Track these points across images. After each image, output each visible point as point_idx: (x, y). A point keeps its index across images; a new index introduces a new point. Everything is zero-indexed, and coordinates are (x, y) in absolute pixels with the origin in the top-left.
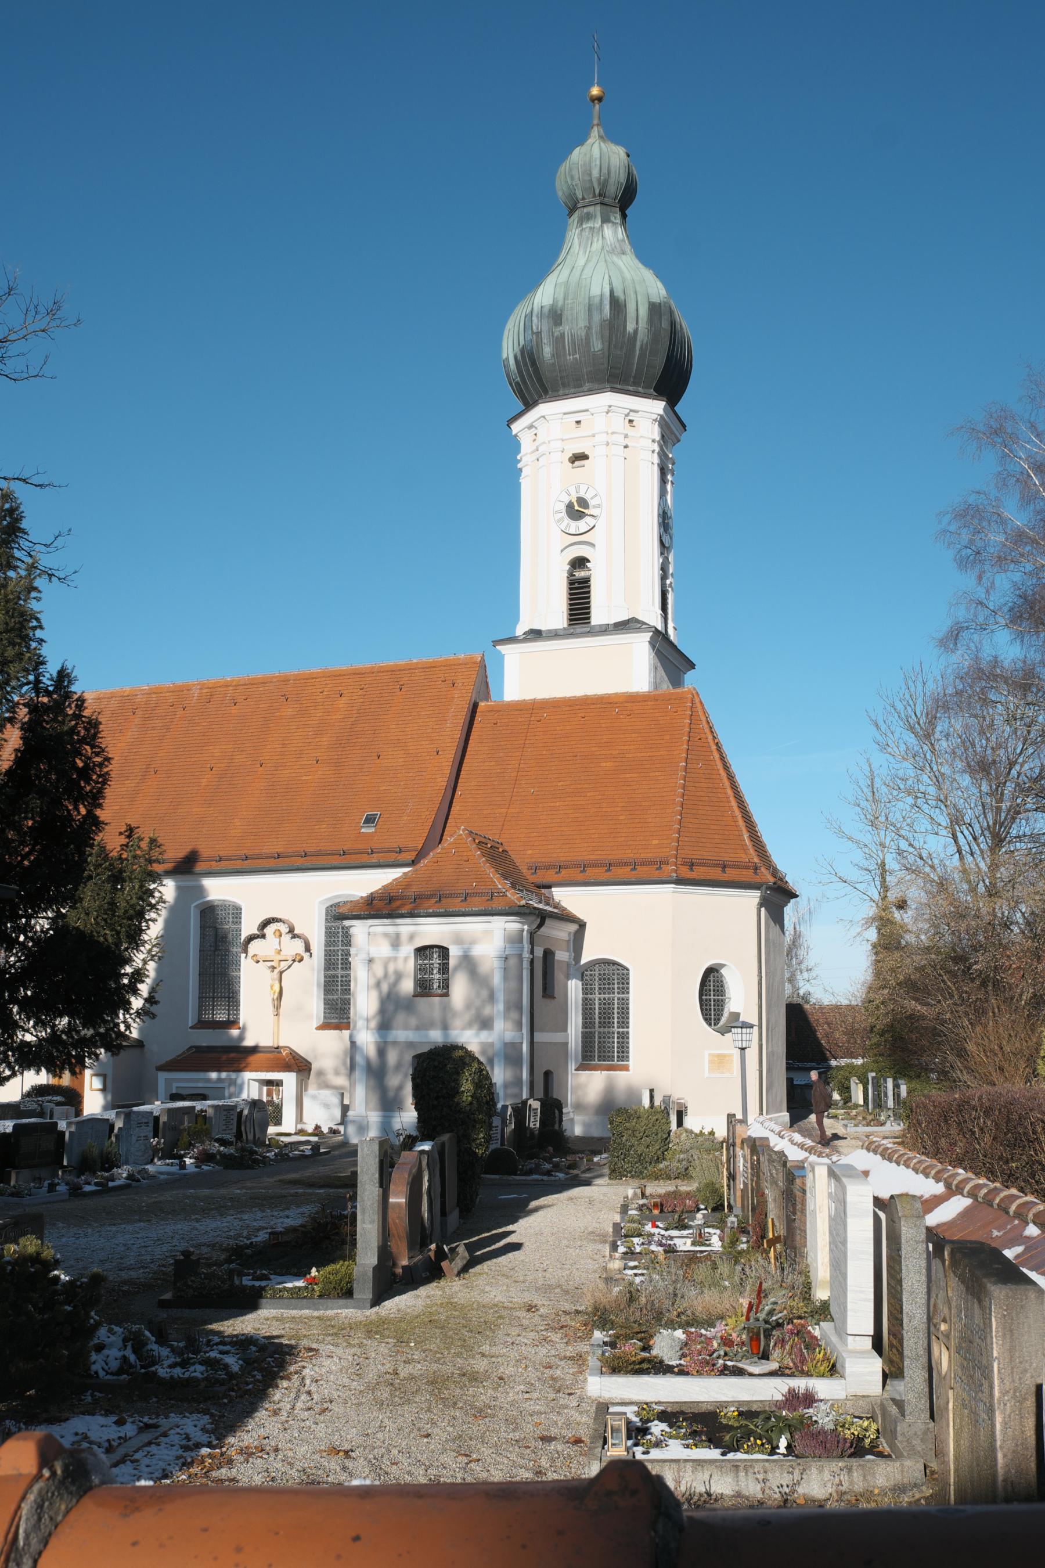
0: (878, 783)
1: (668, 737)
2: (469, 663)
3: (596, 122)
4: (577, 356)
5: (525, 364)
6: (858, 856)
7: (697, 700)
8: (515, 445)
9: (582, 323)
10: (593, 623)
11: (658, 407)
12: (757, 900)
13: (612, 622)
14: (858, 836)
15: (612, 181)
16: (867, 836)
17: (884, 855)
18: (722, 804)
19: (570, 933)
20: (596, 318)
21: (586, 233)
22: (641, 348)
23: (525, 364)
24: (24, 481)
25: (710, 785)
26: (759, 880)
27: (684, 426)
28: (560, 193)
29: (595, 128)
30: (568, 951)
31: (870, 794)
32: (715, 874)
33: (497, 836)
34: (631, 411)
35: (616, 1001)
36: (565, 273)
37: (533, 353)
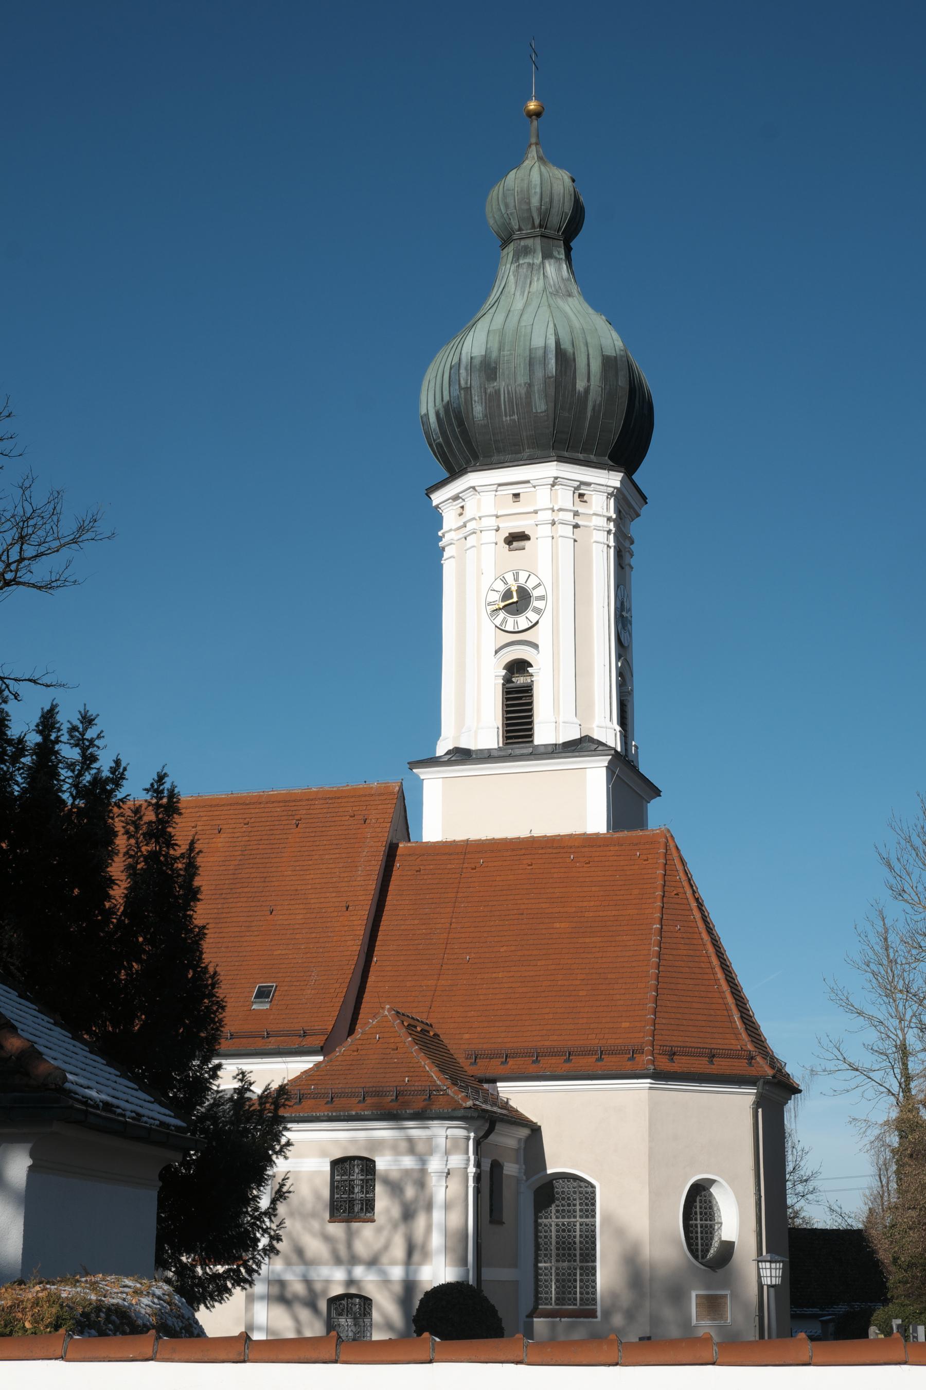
0: (892, 938)
1: (636, 892)
2: (383, 793)
3: (533, 140)
4: (516, 417)
5: (451, 424)
6: (872, 1036)
7: (672, 845)
8: (436, 518)
9: (522, 379)
10: (536, 742)
11: (615, 479)
12: (752, 1098)
13: (561, 742)
14: (871, 1010)
15: (554, 211)
16: (881, 1011)
17: (904, 1035)
18: (706, 977)
19: (520, 1140)
20: (539, 374)
21: (524, 270)
22: (594, 409)
23: (451, 424)
24: (35, 682)
25: (691, 953)
26: (754, 1073)
27: (644, 498)
28: (491, 222)
29: (533, 148)
30: (517, 1163)
31: (881, 951)
32: (700, 1065)
33: (425, 1016)
34: (582, 483)
35: (578, 1227)
36: (499, 319)
37: (460, 412)
